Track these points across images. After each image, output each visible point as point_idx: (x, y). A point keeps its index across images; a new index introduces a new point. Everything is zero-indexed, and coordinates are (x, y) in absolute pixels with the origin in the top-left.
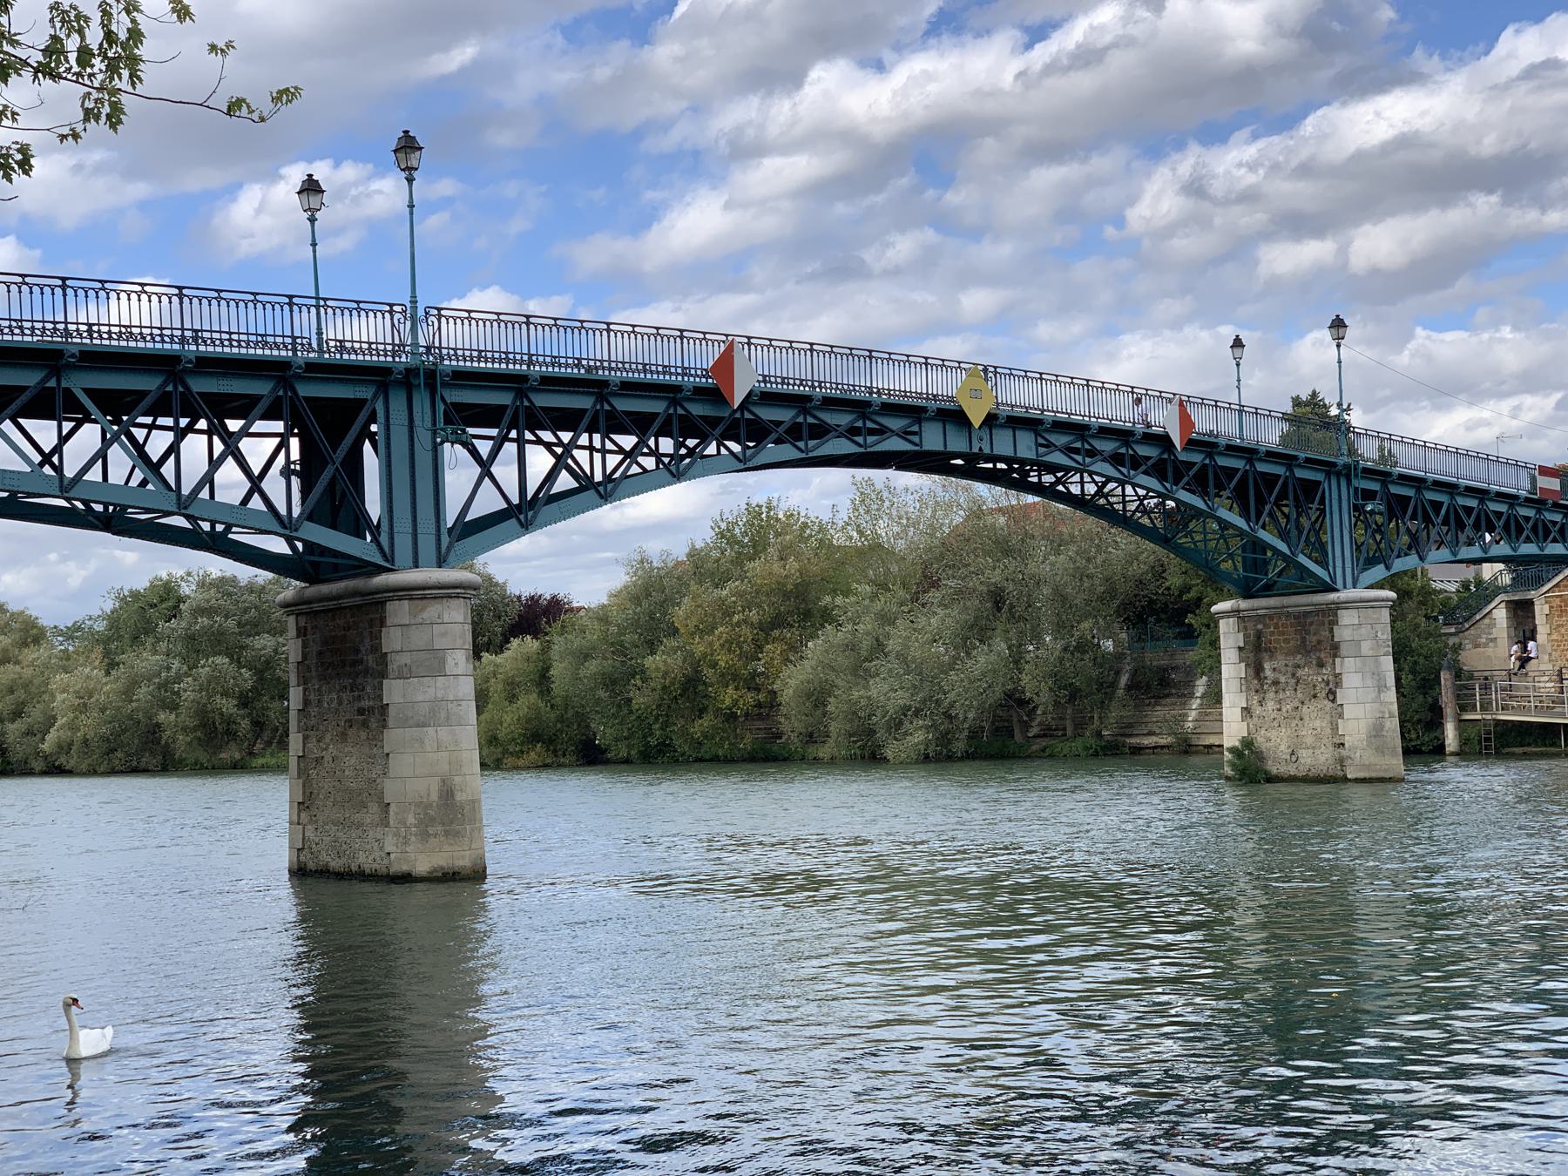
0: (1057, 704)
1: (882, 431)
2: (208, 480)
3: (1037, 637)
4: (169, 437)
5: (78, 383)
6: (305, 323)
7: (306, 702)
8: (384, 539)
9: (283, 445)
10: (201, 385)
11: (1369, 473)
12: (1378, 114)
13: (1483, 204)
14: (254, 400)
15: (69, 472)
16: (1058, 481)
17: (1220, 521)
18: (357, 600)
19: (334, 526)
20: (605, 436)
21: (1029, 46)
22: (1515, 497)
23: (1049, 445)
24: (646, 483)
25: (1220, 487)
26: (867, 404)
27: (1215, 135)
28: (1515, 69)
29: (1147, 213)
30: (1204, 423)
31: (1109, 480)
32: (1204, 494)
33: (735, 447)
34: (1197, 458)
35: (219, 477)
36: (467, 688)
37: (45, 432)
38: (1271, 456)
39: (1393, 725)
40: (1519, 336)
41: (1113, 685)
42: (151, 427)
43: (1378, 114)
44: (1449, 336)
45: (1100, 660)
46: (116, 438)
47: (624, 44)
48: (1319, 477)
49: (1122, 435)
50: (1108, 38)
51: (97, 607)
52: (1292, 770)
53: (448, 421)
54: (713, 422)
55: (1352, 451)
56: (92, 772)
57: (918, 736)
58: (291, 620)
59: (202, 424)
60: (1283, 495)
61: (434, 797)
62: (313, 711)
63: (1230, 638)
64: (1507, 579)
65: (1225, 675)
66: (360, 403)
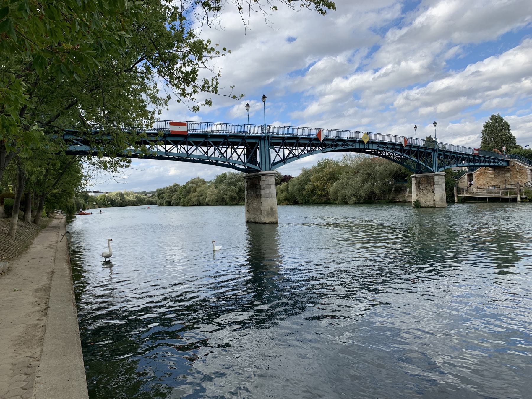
0: (380, 193)
1: (348, 145)
2: (231, 156)
3: (377, 182)
4: (225, 149)
5: (210, 140)
6: (247, 129)
7: (248, 194)
8: (260, 166)
9: (244, 150)
10: (230, 140)
11: (441, 150)
12: (442, 83)
13: (463, 99)
14: (239, 142)
15: (209, 155)
16: (381, 153)
17: (412, 160)
18: (256, 176)
19: (252, 164)
20: (298, 147)
21: (375, 73)
22: (469, 154)
23: (379, 147)
24: (305, 155)
25: (412, 153)
26: (378, 142)
27: (410, 88)
28: (470, 73)
29: (397, 103)
30: (410, 141)
31: (391, 153)
32: (409, 155)
33: (321, 149)
34: (408, 148)
35: (233, 156)
36: (275, 191)
37: (205, 148)
38: (422, 148)
39: (445, 197)
40: (470, 124)
41: (391, 190)
42: (222, 147)
43: (442, 83)
44: (456, 124)
45: (389, 185)
46: (216, 149)
47: (300, 77)
48: (431, 151)
49: (394, 144)
50: (390, 71)
51: (213, 178)
52: (425, 206)
53: (271, 145)
54: (317, 144)
55: (438, 146)
56: (214, 205)
57: (354, 199)
58: (245, 180)
59: (230, 147)
60: (424, 155)
61: (269, 209)
62: (249, 195)
63: (414, 181)
64: (467, 170)
65: (413, 188)
66: (256, 142)
